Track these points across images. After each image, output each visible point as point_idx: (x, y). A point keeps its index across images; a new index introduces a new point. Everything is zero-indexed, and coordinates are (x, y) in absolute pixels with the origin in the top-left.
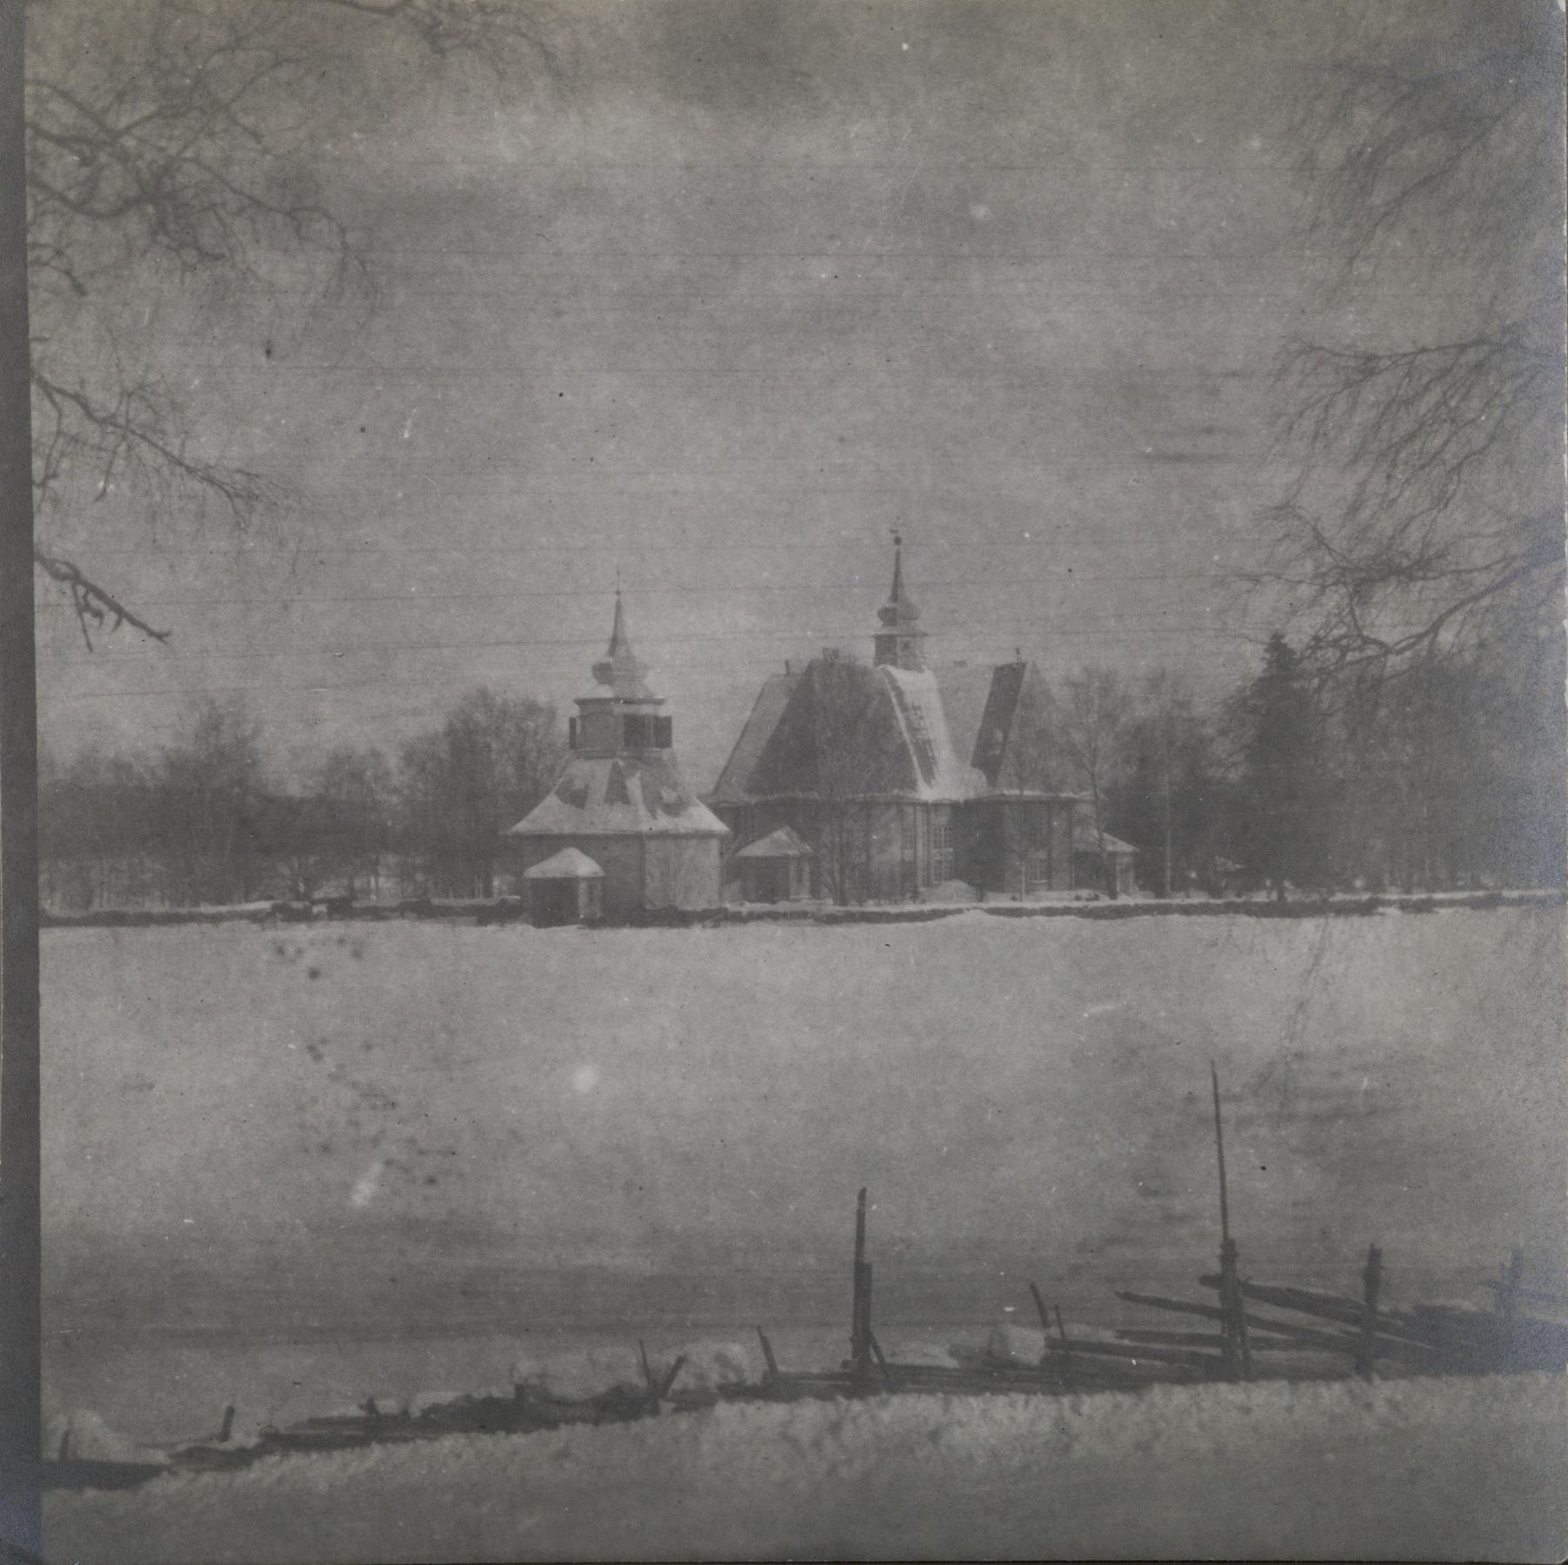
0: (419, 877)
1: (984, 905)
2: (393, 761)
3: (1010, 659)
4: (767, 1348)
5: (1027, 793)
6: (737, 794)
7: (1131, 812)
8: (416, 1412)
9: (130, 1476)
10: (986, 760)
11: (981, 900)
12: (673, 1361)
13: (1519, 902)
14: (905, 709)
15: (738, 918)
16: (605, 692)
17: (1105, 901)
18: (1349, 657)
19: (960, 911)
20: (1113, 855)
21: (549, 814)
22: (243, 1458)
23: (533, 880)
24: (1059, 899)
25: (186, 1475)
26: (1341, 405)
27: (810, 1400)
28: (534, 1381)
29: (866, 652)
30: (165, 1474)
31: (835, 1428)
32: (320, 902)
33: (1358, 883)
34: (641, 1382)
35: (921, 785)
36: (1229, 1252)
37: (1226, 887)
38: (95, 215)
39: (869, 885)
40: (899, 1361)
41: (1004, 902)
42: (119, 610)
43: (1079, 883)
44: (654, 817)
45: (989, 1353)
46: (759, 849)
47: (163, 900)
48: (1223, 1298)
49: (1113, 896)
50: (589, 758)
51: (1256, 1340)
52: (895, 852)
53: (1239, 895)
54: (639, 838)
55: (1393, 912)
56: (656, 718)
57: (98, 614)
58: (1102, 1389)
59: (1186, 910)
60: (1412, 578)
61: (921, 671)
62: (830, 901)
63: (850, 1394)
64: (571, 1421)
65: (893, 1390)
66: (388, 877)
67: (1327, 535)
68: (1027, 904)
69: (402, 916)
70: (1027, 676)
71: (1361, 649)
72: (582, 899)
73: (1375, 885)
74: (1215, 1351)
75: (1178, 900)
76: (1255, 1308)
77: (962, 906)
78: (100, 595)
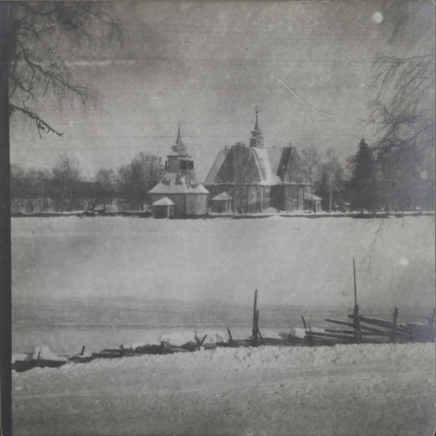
1: (280, 214)
3: (288, 146)
4: (229, 332)
7: (321, 189)
10: (280, 173)
11: (278, 213)
15: (212, 217)
16: (175, 154)
17: (313, 213)
19: (272, 216)
20: (315, 201)
21: (158, 189)
22: (88, 360)
23: (155, 206)
25: (72, 364)
28: (166, 340)
29: (248, 144)
30: (67, 364)
31: (249, 355)
32: (97, 211)
36: (356, 308)
37: (346, 210)
40: (265, 337)
41: (284, 213)
42: (50, 128)
43: (305, 208)
46: (217, 198)
48: (354, 321)
49: (315, 212)
51: (363, 333)
52: (255, 200)
54: (184, 195)
56: (189, 161)
57: (43, 128)
59: (335, 216)
61: (262, 149)
62: (237, 213)
63: (253, 346)
67: (388, 109)
68: (291, 214)
69: (119, 215)
70: (292, 150)
72: (168, 211)
75: (333, 213)
76: (362, 323)
77: (274, 214)
78: (44, 123)
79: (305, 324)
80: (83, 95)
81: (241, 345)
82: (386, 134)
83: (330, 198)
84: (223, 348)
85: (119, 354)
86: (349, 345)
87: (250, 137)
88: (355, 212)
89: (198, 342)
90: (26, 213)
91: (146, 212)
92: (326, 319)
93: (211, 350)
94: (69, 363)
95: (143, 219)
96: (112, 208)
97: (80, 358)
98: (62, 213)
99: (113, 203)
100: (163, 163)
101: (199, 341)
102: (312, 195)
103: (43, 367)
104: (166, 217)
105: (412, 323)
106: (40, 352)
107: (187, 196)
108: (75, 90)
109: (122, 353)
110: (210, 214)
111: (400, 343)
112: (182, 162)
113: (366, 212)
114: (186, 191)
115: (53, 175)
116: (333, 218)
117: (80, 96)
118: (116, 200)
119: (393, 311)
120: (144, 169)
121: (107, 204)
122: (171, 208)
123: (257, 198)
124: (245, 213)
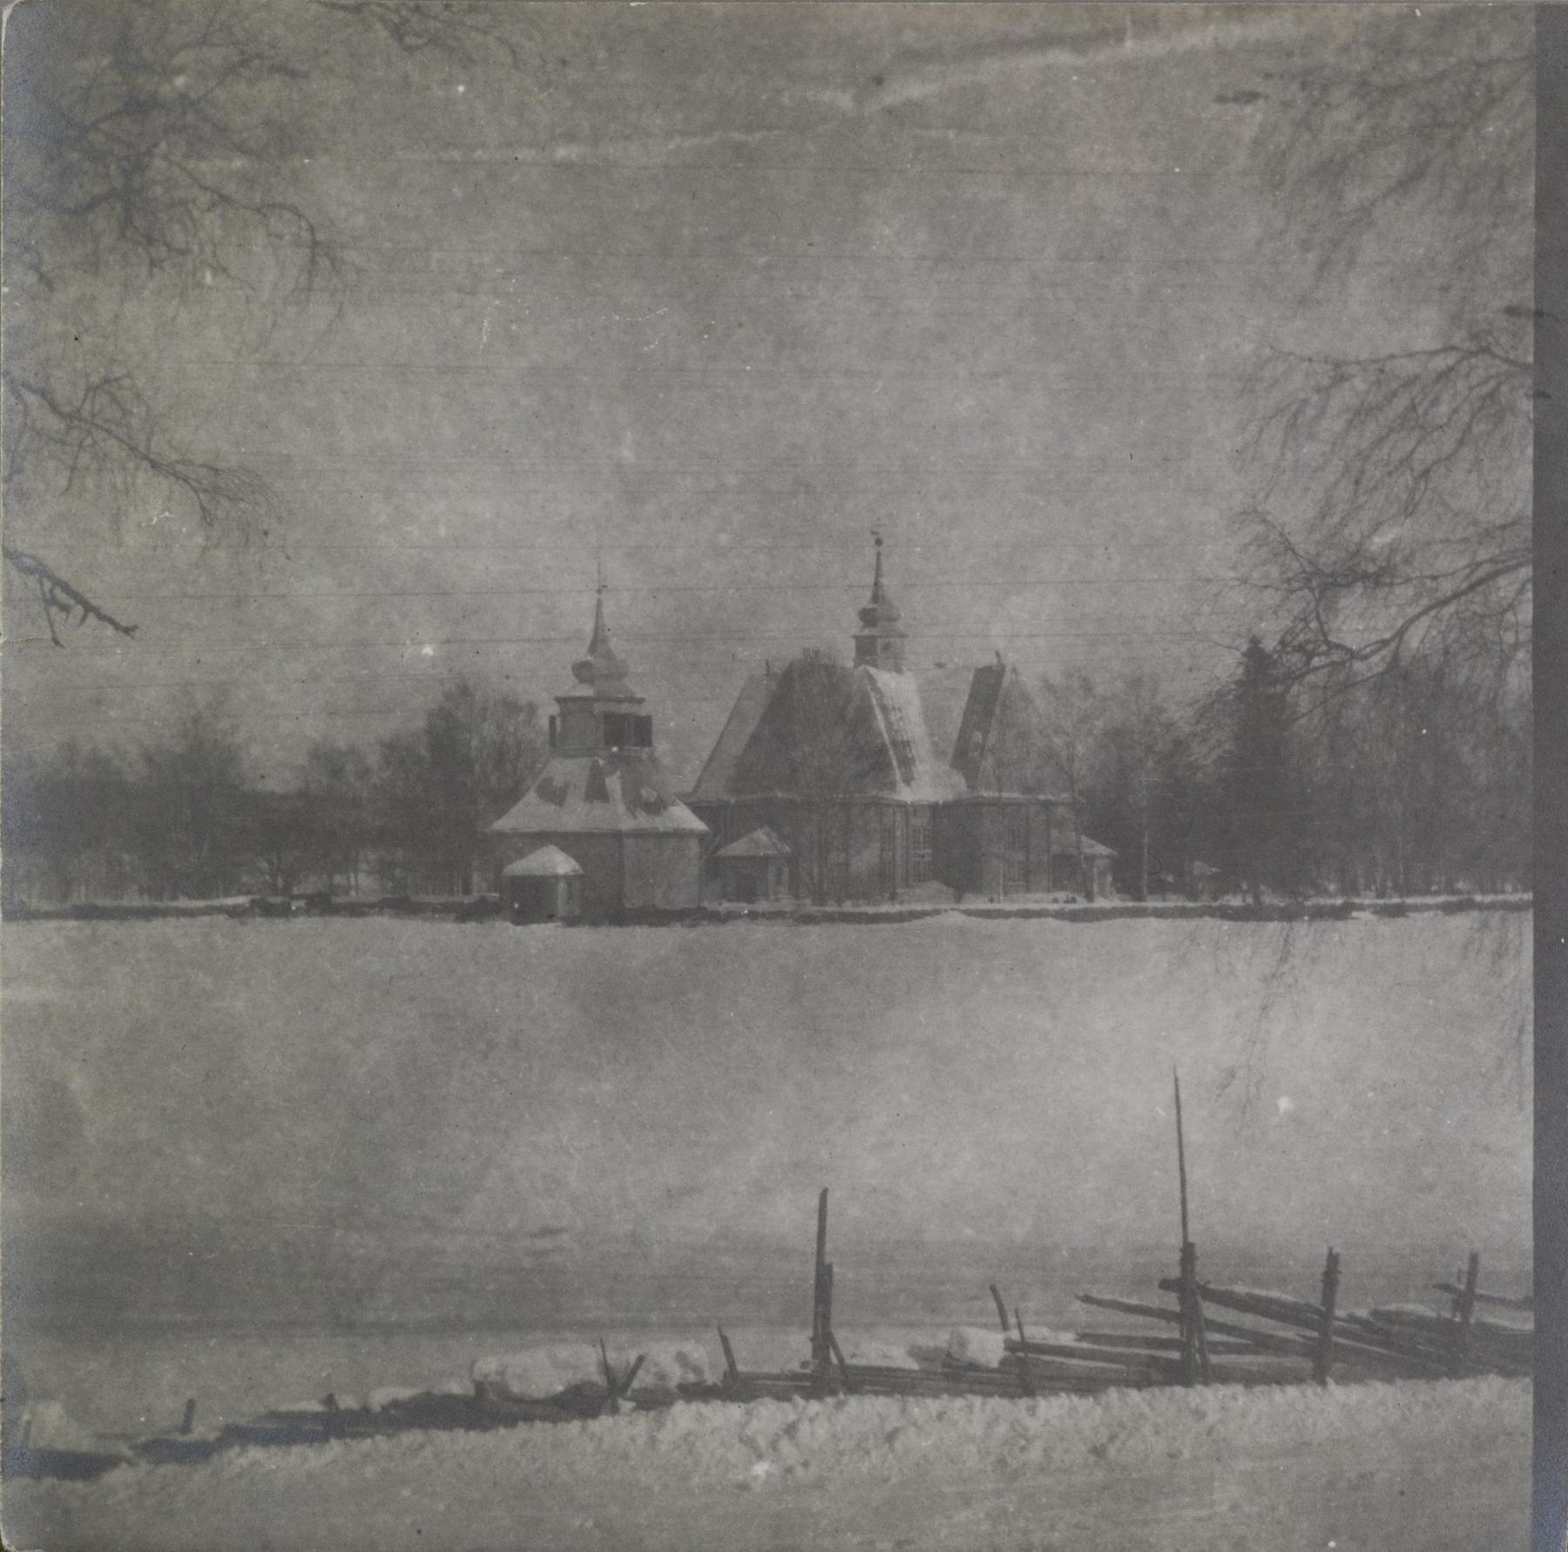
0: (398, 872)
1: (962, 907)
2: (373, 760)
5: (1005, 795)
6: (716, 791)
7: (1105, 818)
8: (376, 1408)
10: (963, 757)
11: (959, 899)
13: (1492, 907)
14: (884, 709)
16: (586, 691)
17: (1081, 904)
18: (1316, 661)
19: (923, 914)
20: (1091, 859)
21: (527, 813)
24: (1036, 902)
27: (767, 1400)
28: (494, 1378)
29: (846, 656)
30: (124, 1465)
31: (791, 1430)
32: (298, 897)
33: (1332, 887)
34: (599, 1379)
35: (901, 786)
36: (1188, 1252)
41: (982, 904)
42: (89, 608)
45: (949, 1355)
46: (738, 848)
48: (1182, 1300)
49: (1089, 897)
50: (567, 756)
54: (618, 836)
56: (637, 717)
57: (65, 608)
58: (1054, 1391)
59: (1160, 914)
60: (1377, 584)
62: (808, 901)
64: (529, 1419)
66: (369, 873)
69: (381, 913)
70: (1006, 681)
71: (1327, 654)
73: (1349, 888)
74: (1175, 1355)
75: (1152, 903)
76: (1210, 1310)
78: (66, 588)
87: (855, 631)
88: (1235, 901)
89: (612, 1380)
90: (45, 906)
93: (652, 1414)
95: (470, 926)
96: (357, 888)
98: (174, 904)
104: (551, 917)
105: (1393, 1307)
111: (1343, 1380)
112: (609, 717)
113: (1270, 899)
114: (627, 824)
117: (192, 494)
119: (1321, 1267)
122: (569, 885)
124: (840, 903)
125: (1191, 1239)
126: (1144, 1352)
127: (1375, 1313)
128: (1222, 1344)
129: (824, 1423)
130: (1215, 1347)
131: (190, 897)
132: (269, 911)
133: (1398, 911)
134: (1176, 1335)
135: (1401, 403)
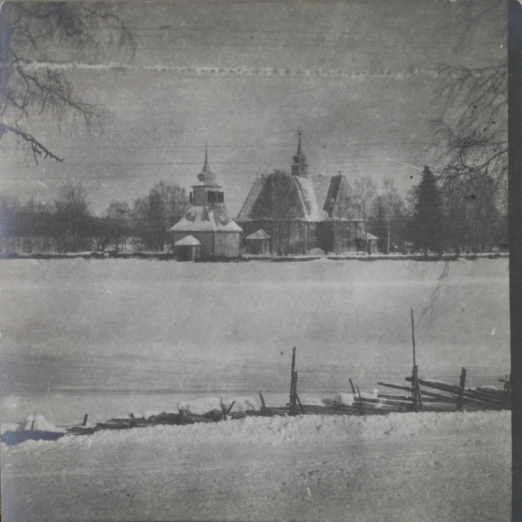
1: (327, 256)
6: (245, 218)
7: (377, 226)
9: (54, 436)
10: (328, 208)
11: (326, 254)
12: (231, 402)
16: (202, 184)
17: (367, 255)
19: (319, 258)
20: (370, 240)
21: (183, 224)
22: (90, 432)
23: (177, 246)
25: (72, 436)
26: (458, 87)
29: (289, 172)
30: (65, 436)
31: (285, 425)
35: (306, 216)
38: (39, 17)
39: (290, 250)
40: (306, 404)
41: (333, 255)
42: (48, 153)
44: (217, 224)
45: (335, 402)
46: (252, 236)
47: (55, 250)
48: (413, 384)
49: (370, 253)
51: (423, 398)
53: (412, 254)
54: (212, 232)
55: (463, 259)
56: (218, 192)
57: (40, 152)
61: (307, 178)
63: (290, 414)
64: (198, 421)
65: (304, 413)
68: (341, 256)
69: (134, 257)
70: (343, 179)
74: (411, 402)
75: (391, 255)
76: (422, 388)
78: (40, 146)
79: (353, 389)
80: (87, 113)
81: (276, 413)
82: (451, 160)
83: (387, 237)
84: (253, 418)
85: (129, 424)
86: (406, 413)
87: (291, 164)
88: (419, 255)
90: (26, 254)
91: (166, 254)
92: (379, 382)
93: (239, 420)
94: (69, 435)
95: (164, 262)
96: (126, 249)
97: (81, 429)
98: (66, 254)
99: (127, 242)
100: (187, 194)
101: (225, 409)
102: (366, 232)
103: (37, 439)
106: (33, 422)
107: (216, 234)
108: (78, 107)
109: (133, 423)
110: (244, 256)
111: (469, 411)
112: (210, 193)
113: (431, 254)
114: (215, 229)
115: (56, 210)
116: (391, 260)
117: (83, 115)
118: (130, 239)
120: (165, 201)
121: (119, 243)
122: (196, 248)
123: (300, 237)
124: (286, 255)
125: (416, 364)
126: (401, 401)
127: (478, 389)
128: (425, 398)
129: (296, 423)
130: (425, 400)
131: (71, 252)
132: (97, 256)
133: (473, 258)
134: (411, 395)
135: (489, 84)
